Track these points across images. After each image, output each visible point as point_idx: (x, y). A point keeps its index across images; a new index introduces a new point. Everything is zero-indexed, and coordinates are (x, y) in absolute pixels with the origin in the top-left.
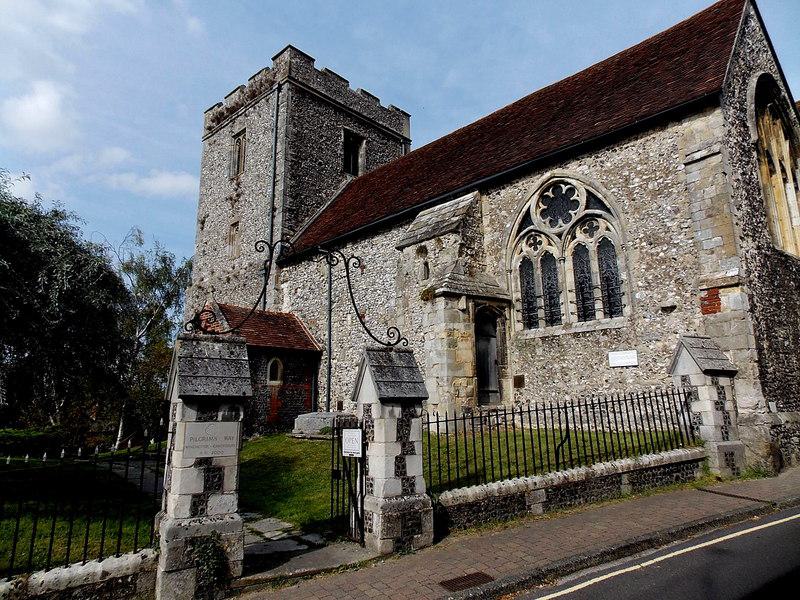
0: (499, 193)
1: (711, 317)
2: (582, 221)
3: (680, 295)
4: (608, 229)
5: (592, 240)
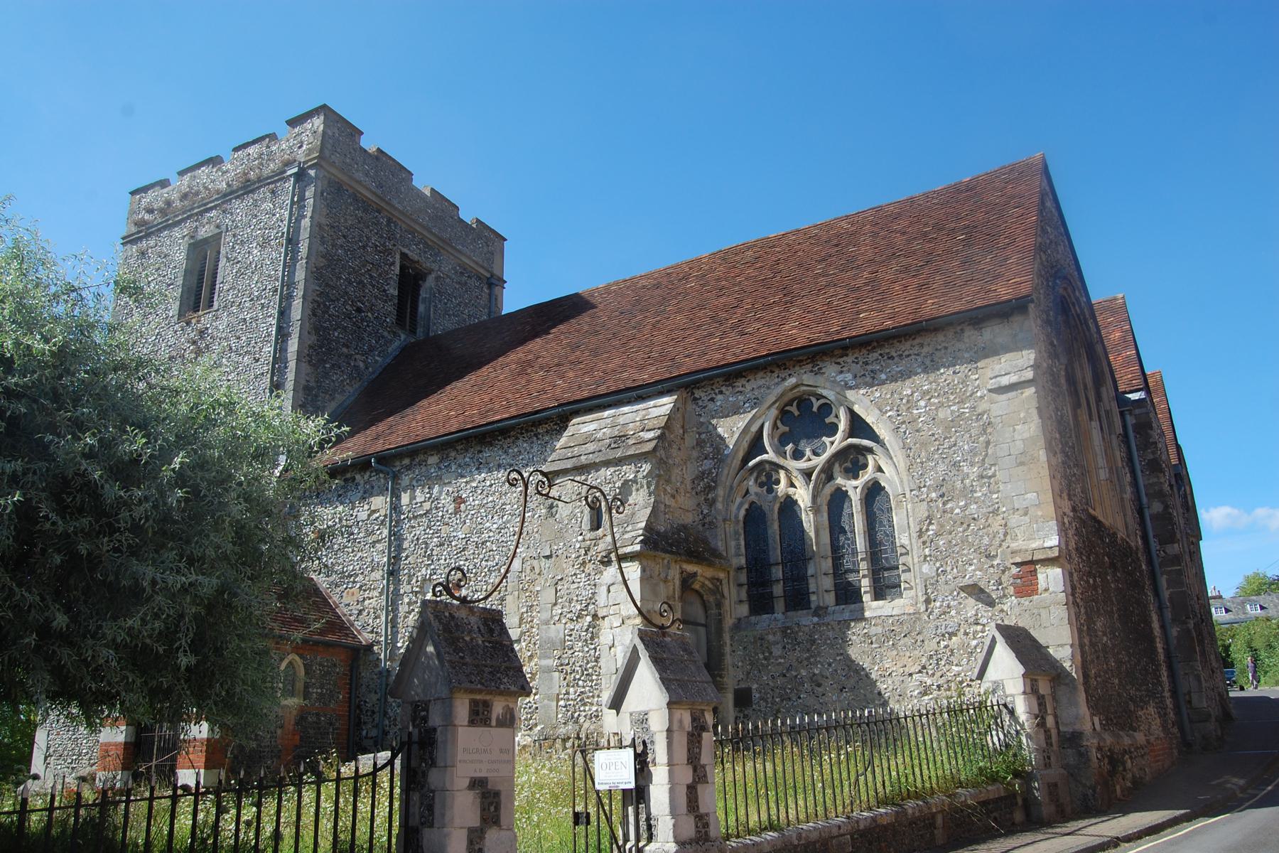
0: (712, 400)
1: (1025, 601)
2: (841, 455)
4: (880, 470)
5: (854, 483)
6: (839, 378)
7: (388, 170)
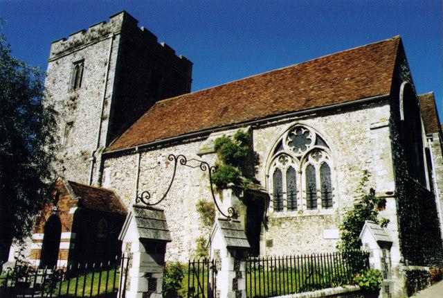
2: (313, 151)
7: (149, 37)
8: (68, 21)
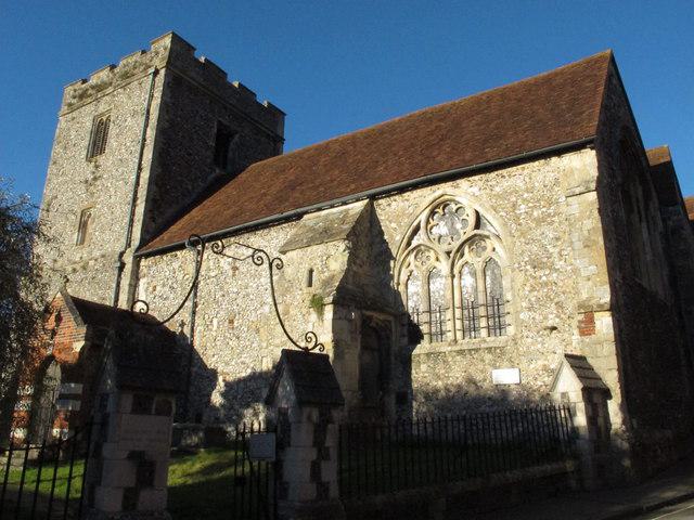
0: (389, 205)
1: (587, 339)
3: (558, 317)
6: (470, 190)
8: (91, 51)
